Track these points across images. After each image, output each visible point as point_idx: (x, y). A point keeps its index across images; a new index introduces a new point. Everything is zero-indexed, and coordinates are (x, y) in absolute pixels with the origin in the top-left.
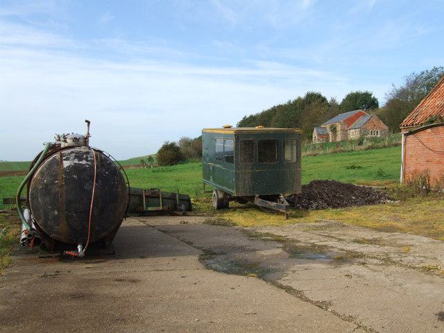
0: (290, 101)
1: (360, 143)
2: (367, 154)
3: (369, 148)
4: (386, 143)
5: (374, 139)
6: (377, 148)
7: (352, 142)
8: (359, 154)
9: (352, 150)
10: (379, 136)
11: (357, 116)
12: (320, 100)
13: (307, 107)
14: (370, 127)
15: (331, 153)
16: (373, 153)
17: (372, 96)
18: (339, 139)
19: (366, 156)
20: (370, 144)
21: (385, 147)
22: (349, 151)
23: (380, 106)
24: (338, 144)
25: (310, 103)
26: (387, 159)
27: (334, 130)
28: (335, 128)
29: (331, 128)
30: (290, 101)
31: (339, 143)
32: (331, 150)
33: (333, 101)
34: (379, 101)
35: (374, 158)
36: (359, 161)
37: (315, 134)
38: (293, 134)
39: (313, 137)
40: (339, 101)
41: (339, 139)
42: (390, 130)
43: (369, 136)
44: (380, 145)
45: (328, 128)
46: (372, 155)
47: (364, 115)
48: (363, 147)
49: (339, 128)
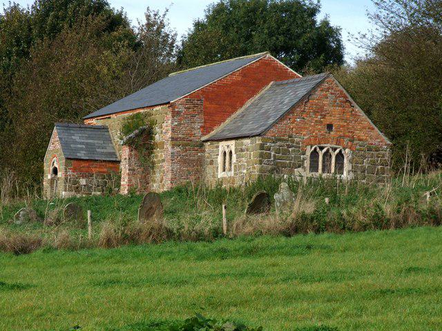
0: (107, 4)
1: (260, 200)
2: (282, 251)
3: (295, 229)
4: (388, 209)
5: (328, 189)
6: (343, 227)
7: (219, 196)
8: (251, 252)
9: (217, 234)
10: (346, 176)
11: (252, 81)
12: (99, 20)
13: (40, 47)
14: (305, 132)
15: (109, 243)
16: (327, 249)
17: (319, 18)
18: (162, 181)
19: (293, 264)
20: (309, 208)
21: (380, 223)
22: (199, 237)
23: (354, 52)
24: (149, 202)
25: (55, 29)
26: (407, 281)
27: (142, 139)
28: (148, 134)
29: (127, 129)
30: (313, 12)
31: (156, 197)
32: (107, 228)
33: (154, 26)
34: (344, 38)
35: (336, 277)
36: (247, 288)
37: (54, 157)
38: (84, 227)
39: (48, 169)
40: (180, 27)
41: (162, 181)
42: (397, 148)
43: (303, 173)
44: (357, 213)
45: (116, 135)
46: (317, 262)
47: (281, 76)
48: (272, 219)
49: (164, 132)
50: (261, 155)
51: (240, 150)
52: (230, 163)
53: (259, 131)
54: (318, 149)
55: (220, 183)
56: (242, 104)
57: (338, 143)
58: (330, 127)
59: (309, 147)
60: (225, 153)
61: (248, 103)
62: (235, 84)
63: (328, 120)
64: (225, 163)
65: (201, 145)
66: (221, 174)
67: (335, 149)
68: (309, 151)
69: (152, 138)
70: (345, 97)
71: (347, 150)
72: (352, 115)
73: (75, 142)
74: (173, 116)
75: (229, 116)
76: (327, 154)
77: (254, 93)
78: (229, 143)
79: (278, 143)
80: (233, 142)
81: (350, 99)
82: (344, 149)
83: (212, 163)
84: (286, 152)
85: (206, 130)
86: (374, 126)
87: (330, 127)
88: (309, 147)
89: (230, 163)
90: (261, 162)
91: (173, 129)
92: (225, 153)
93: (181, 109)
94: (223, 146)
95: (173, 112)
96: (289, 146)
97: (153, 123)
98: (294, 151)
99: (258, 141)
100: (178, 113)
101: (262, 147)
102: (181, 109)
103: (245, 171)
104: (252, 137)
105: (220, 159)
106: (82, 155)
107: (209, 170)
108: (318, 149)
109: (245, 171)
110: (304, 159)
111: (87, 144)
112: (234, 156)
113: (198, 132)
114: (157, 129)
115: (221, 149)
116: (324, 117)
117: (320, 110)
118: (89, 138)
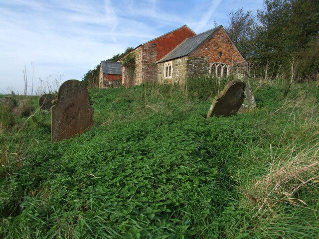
18: (139, 79)
39: (100, 78)
50: (188, 66)
51: (175, 65)
52: (170, 73)
53: (186, 54)
54: (215, 65)
55: (166, 81)
56: (174, 48)
57: (225, 61)
58: (221, 53)
59: (211, 63)
60: (167, 68)
61: (177, 47)
62: (171, 38)
63: (220, 50)
64: (167, 72)
65: (156, 65)
66: (166, 78)
67: (223, 65)
68: (211, 65)
69: (135, 63)
70: (228, 39)
71: (228, 66)
72: (231, 48)
73: (108, 68)
74: (143, 51)
75: (169, 52)
76: (219, 68)
77: (180, 42)
78: (169, 62)
79: (196, 60)
80: (171, 62)
81: (230, 40)
82: (227, 65)
83: (161, 73)
84: (200, 65)
85: (158, 58)
86: (240, 54)
87: (221, 53)
88: (211, 63)
89: (170, 73)
90: (187, 70)
91: (143, 57)
92: (167, 68)
93: (147, 48)
94: (166, 64)
95: (143, 49)
96: (201, 62)
97: (135, 56)
98: (204, 65)
99: (186, 59)
100: (145, 50)
101: (188, 62)
102: (147, 48)
103: (178, 75)
104: (183, 57)
105: (165, 71)
106: (110, 72)
107: (159, 76)
108: (215, 65)
109: (178, 75)
110: (209, 70)
111: (113, 69)
112: (172, 68)
113: (155, 59)
114: (137, 59)
115: (165, 66)
116: (218, 48)
117: (216, 44)
118: (113, 66)
